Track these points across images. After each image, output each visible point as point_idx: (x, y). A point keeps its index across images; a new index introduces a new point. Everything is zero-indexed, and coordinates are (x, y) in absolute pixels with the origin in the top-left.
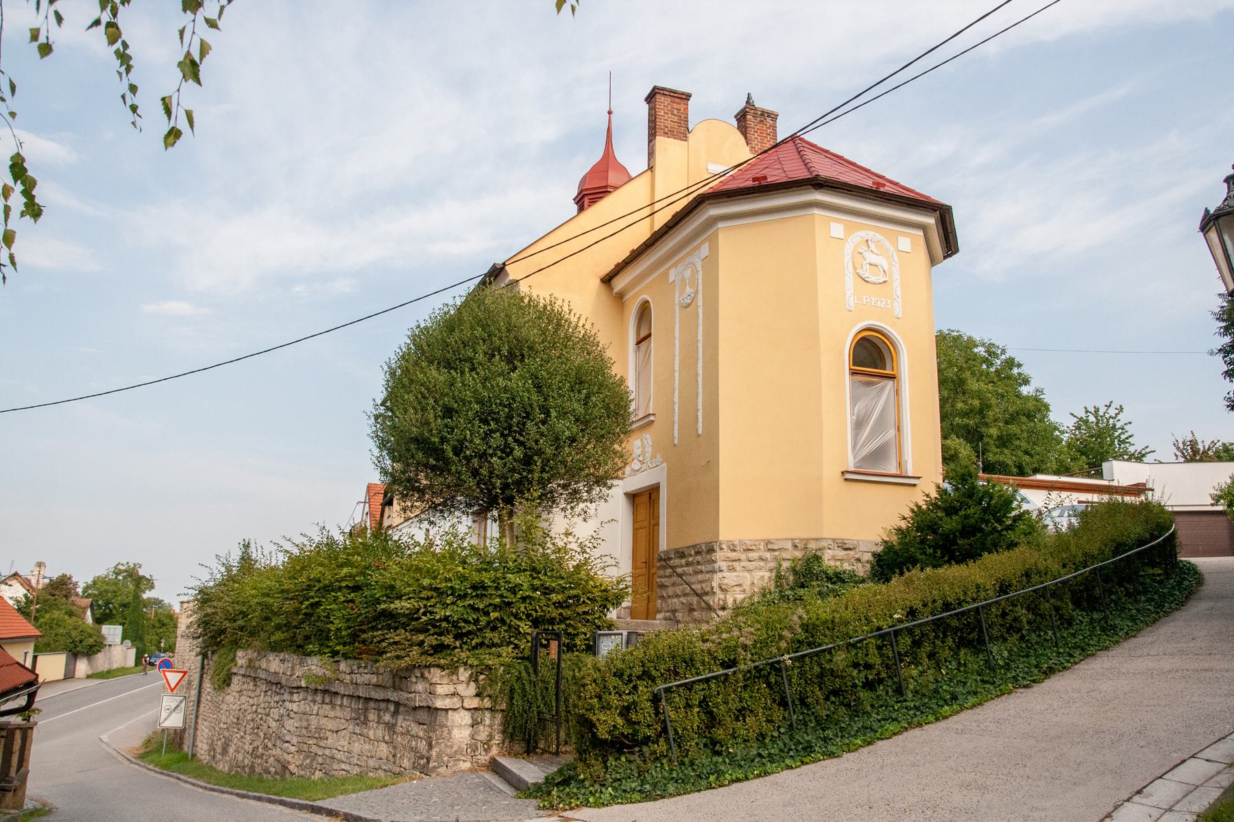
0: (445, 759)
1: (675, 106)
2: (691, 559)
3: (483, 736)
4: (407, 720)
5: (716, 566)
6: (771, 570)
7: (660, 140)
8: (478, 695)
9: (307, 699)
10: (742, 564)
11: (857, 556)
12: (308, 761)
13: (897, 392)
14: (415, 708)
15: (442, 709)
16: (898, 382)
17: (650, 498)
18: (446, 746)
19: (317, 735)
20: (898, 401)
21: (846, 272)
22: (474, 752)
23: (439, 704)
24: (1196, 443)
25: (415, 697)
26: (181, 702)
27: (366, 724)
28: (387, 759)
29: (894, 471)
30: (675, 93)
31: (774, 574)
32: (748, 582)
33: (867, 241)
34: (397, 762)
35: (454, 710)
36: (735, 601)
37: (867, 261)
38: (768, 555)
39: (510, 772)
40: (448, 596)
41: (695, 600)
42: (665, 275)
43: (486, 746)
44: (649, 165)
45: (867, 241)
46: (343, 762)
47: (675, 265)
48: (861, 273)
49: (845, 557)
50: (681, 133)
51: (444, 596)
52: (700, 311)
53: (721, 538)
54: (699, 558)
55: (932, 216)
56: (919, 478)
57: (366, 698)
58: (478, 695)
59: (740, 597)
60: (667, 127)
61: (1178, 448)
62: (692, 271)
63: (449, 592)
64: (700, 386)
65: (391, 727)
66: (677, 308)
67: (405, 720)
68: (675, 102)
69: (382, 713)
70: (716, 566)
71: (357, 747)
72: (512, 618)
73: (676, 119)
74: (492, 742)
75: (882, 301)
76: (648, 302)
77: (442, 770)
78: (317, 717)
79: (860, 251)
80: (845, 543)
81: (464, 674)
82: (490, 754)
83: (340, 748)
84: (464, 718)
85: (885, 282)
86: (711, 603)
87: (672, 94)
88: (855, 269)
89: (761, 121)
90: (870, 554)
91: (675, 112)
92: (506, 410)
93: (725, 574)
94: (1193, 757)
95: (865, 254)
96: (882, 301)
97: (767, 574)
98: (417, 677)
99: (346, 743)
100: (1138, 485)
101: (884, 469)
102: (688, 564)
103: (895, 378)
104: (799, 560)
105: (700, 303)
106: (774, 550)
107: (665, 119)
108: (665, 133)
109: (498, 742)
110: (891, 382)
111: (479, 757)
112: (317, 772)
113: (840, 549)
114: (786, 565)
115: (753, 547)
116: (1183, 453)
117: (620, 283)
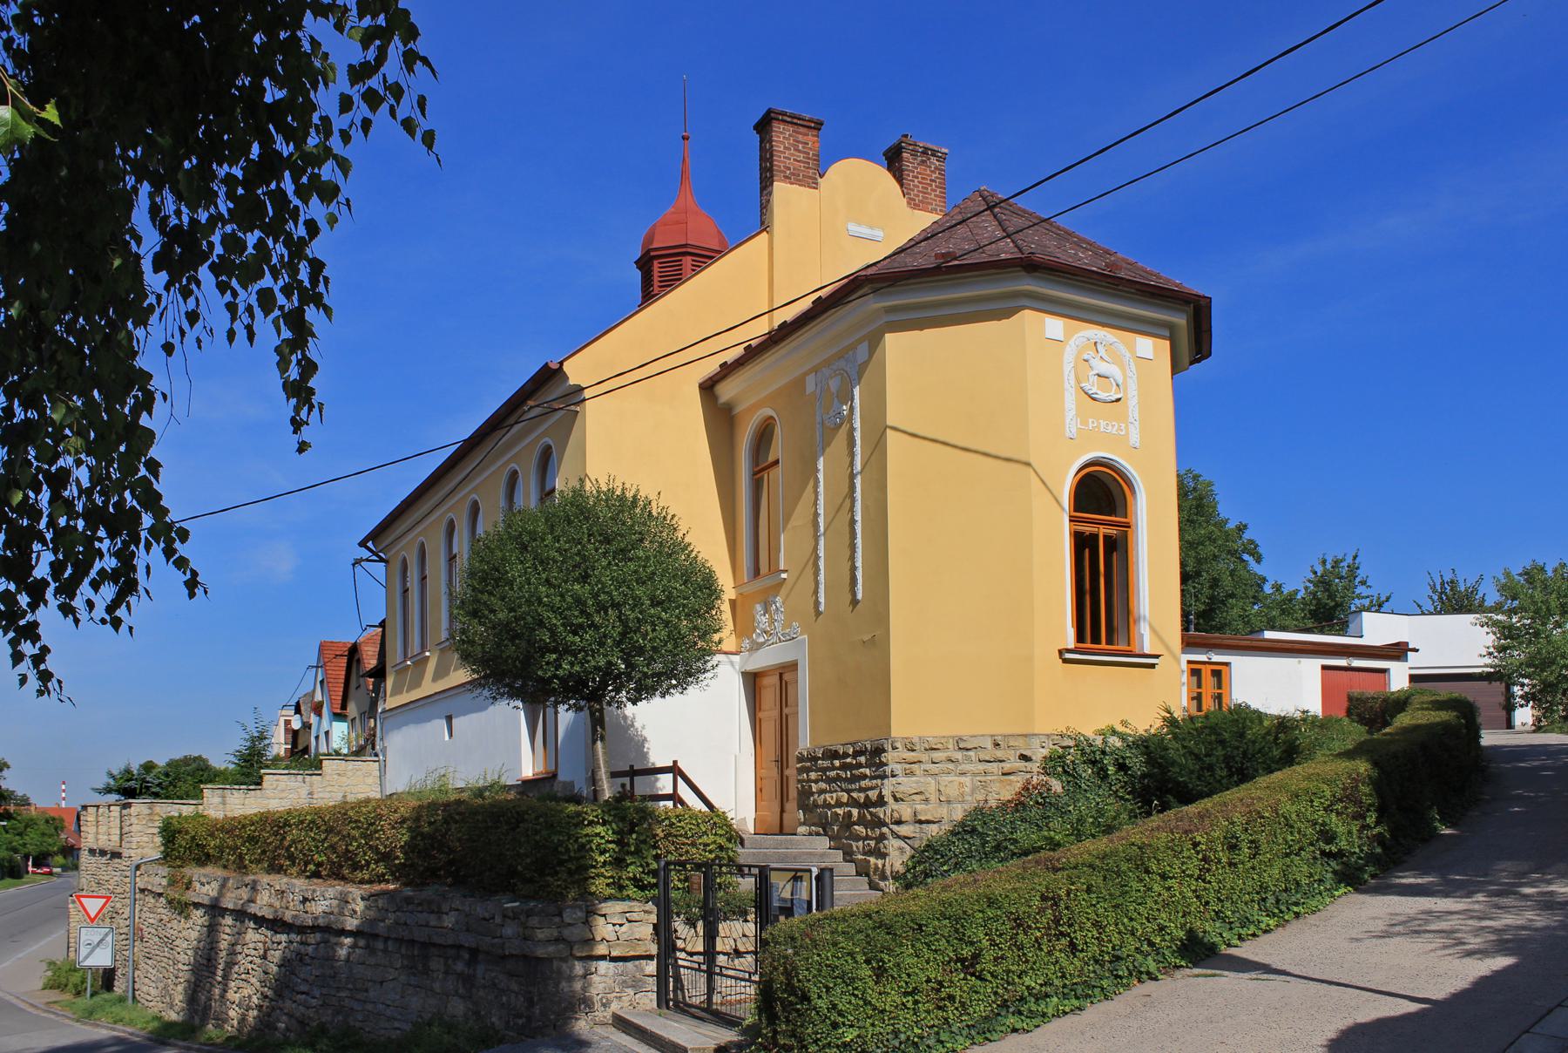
1: (800, 137)
5: (888, 770)
10: (923, 766)
12: (341, 1018)
14: (504, 957)
19: (350, 986)
23: (540, 952)
26: (107, 935)
30: (799, 119)
33: (1096, 343)
37: (1096, 372)
46: (395, 1019)
50: (810, 178)
53: (893, 734)
55: (1183, 311)
60: (789, 169)
61: (1434, 591)
65: (468, 980)
69: (450, 962)
70: (888, 770)
71: (415, 1002)
73: (801, 157)
75: (1113, 426)
79: (1086, 357)
83: (389, 1002)
86: (882, 816)
88: (1078, 381)
89: (923, 162)
91: (800, 148)
93: (899, 780)
94: (1559, 1005)
95: (1092, 362)
100: (1398, 644)
108: (786, 177)
115: (939, 746)
117: (726, 391)
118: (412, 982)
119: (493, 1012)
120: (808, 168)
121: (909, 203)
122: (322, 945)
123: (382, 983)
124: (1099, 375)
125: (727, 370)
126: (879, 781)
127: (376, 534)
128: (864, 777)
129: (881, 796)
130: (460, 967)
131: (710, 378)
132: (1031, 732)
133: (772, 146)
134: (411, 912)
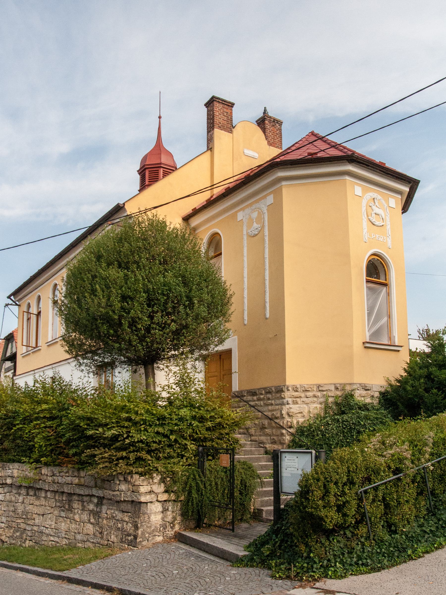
0: (147, 535)
1: (225, 110)
2: (262, 397)
3: (169, 518)
4: (112, 509)
5: (285, 401)
6: (321, 403)
7: (217, 132)
8: (166, 491)
9: (11, 492)
11: (372, 394)
12: (18, 534)
13: (388, 294)
14: (118, 502)
15: (144, 503)
16: (389, 287)
17: (220, 358)
18: (147, 527)
19: (24, 517)
20: (389, 299)
21: (364, 218)
22: (165, 529)
23: (143, 499)
24: (429, 331)
25: (121, 494)
27: (71, 511)
28: (94, 534)
29: (386, 343)
30: (225, 102)
31: (323, 405)
32: (306, 411)
33: (374, 199)
34: (104, 537)
35: (151, 502)
36: (298, 422)
37: (374, 212)
38: (319, 394)
39: (203, 543)
40: (141, 425)
41: (266, 422)
42: (235, 216)
43: (172, 525)
44: (208, 147)
45: (374, 199)
47: (243, 209)
48: (371, 219)
49: (366, 395)
50: (229, 128)
51: (138, 425)
52: (267, 239)
53: (287, 383)
54: (269, 396)
56: (402, 346)
57: (68, 493)
58: (166, 491)
59: (301, 420)
61: (420, 333)
62: (259, 213)
63: (142, 423)
64: (268, 287)
65: (96, 514)
66: (245, 237)
67: (108, 509)
68: (225, 108)
69: (85, 504)
70: (285, 401)
71: (63, 526)
72: (182, 439)
74: (176, 522)
75: (381, 237)
76: (217, 233)
77: (144, 543)
78: (23, 505)
79: (371, 205)
80: (366, 386)
81: (157, 478)
82: (174, 530)
83: (47, 526)
84: (158, 507)
85: (383, 225)
86: (281, 424)
87: (223, 102)
88: (368, 216)
90: (378, 393)
91: (225, 114)
92: (165, 298)
93: (291, 406)
96: (381, 237)
97: (319, 406)
98: (120, 480)
99: (53, 523)
101: (382, 341)
102: (259, 400)
103: (387, 285)
104: (340, 397)
105: (266, 233)
106: (323, 391)
107: (219, 118)
108: (220, 127)
109: (179, 522)
110: (385, 288)
111: (167, 532)
112: (28, 542)
113: (363, 390)
114: (331, 400)
115: (310, 389)
116: (422, 336)
117: (194, 222)
118: (62, 515)
119: (112, 532)
120: (228, 124)
121: (268, 143)
122: (8, 494)
123: (43, 515)
124: (376, 214)
125: (196, 212)
126: (280, 407)
127: (15, 293)
128: (272, 404)
129: (282, 415)
130: (91, 507)
131: (189, 215)
132: (352, 382)
133: (214, 113)
134: (62, 476)
